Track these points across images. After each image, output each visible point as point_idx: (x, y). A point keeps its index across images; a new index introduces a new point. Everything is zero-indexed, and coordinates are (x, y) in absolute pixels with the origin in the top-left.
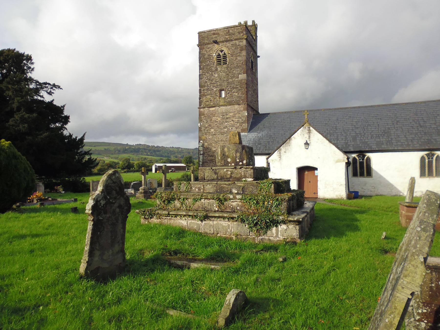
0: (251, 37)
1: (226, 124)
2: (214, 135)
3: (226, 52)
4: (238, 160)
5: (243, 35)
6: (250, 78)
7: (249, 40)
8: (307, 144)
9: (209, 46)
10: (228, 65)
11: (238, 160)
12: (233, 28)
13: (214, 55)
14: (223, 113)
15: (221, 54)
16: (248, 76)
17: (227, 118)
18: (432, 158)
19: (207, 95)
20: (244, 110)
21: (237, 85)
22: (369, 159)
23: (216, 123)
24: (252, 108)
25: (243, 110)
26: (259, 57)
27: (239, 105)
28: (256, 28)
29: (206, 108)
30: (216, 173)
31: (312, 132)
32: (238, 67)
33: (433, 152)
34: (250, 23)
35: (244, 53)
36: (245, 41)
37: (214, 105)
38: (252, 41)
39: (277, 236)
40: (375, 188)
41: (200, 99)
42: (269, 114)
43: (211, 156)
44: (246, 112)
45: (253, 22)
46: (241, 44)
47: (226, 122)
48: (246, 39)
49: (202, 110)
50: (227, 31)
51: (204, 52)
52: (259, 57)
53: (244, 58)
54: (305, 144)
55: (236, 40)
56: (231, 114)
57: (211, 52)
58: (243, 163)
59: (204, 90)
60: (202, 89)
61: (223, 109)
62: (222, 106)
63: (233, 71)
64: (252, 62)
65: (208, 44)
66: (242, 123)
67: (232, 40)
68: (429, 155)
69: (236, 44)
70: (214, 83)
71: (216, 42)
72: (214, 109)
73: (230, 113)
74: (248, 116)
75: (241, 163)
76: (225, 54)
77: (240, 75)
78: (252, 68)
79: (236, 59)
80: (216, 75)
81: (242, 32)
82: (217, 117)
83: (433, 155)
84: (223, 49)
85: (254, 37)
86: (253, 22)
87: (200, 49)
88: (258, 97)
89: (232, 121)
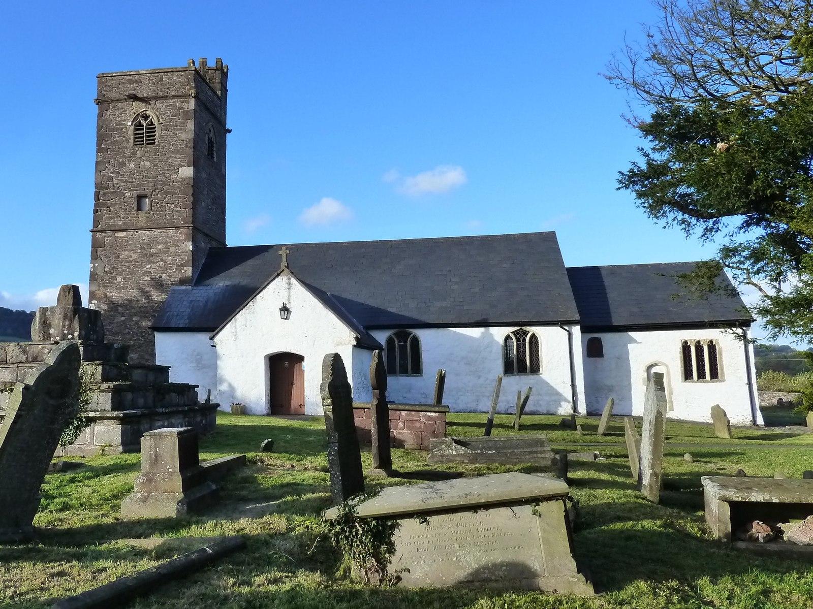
0: (210, 93)
1: (149, 266)
2: (123, 288)
3: (155, 121)
4: (66, 332)
5: (189, 90)
6: (204, 175)
7: (204, 98)
8: (285, 309)
9: (120, 105)
10: (158, 145)
11: (66, 332)
12: (169, 74)
13: (130, 123)
14: (143, 243)
15: (144, 123)
16: (197, 171)
17: (152, 255)
18: (524, 340)
19: (112, 205)
20: (187, 239)
21: (174, 189)
22: (416, 342)
23: (127, 264)
24: (207, 235)
25: (185, 240)
26: (229, 131)
27: (177, 228)
28: (225, 75)
29: (109, 233)
30: (25, 352)
31: (293, 286)
32: (176, 152)
33: (524, 328)
34: (212, 64)
35: (191, 125)
36: (192, 102)
37: (123, 227)
38: (212, 101)
39: (91, 443)
40: (426, 397)
41: (96, 211)
42: (272, 246)
43: (113, 334)
44: (191, 243)
45: (219, 61)
46: (185, 106)
47: (150, 262)
48: (195, 97)
49: (98, 235)
50: (158, 79)
51: (107, 115)
52: (229, 131)
53: (191, 136)
54: (281, 310)
55: (175, 97)
56: (159, 247)
57: (123, 118)
58: (73, 335)
59: (104, 194)
60: (101, 192)
61: (144, 235)
62: (142, 228)
63: (168, 159)
64: (211, 142)
65: (119, 100)
66: (182, 265)
67: (166, 97)
68: (518, 333)
69: (174, 106)
70: (127, 182)
71: (135, 98)
72: (124, 234)
73: (159, 243)
74: (194, 253)
75: (70, 337)
76: (152, 124)
77: (180, 169)
78: (211, 153)
79: (175, 134)
80: (132, 166)
81: (188, 84)
82: (130, 251)
83: (526, 333)
84: (148, 113)
85: (219, 93)
86: (219, 61)
87: (101, 110)
88: (224, 212)
89: (162, 260)
